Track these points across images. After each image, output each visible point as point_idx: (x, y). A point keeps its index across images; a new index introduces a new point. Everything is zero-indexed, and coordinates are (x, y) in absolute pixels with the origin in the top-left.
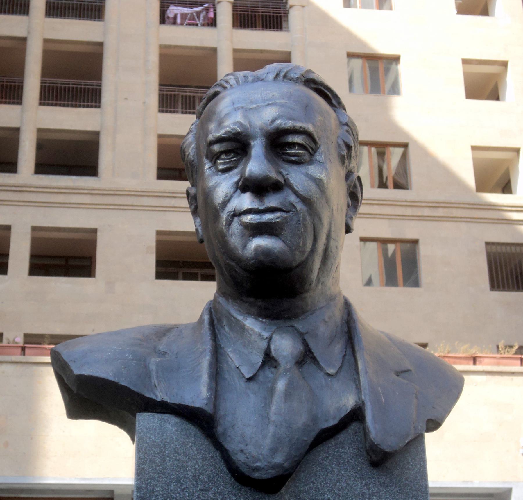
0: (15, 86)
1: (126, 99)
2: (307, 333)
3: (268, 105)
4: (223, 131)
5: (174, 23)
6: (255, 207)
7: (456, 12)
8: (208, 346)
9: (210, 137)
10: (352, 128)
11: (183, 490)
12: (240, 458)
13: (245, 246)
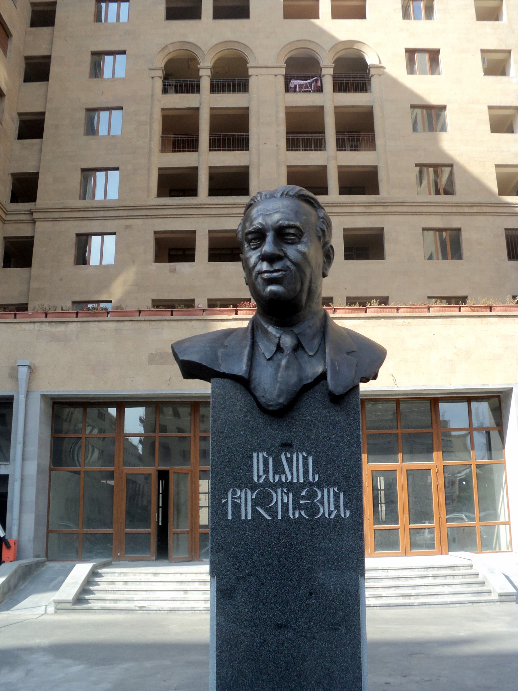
0: (193, 140)
1: (265, 143)
2: (299, 334)
3: (276, 212)
4: (252, 228)
5: (295, 91)
6: (268, 269)
7: (483, 74)
8: (249, 342)
9: (246, 231)
10: (326, 219)
11: (235, 416)
12: (262, 400)
13: (264, 290)
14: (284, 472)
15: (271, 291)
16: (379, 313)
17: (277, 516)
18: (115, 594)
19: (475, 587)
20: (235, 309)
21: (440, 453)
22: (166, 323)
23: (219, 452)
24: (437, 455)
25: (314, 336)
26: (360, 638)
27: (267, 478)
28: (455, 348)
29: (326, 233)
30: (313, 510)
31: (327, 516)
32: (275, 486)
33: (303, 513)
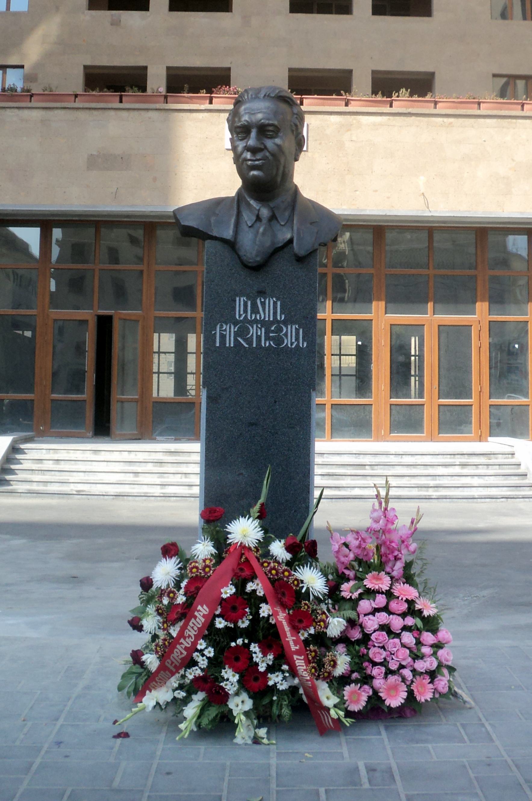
3: (259, 112)
4: (240, 124)
12: (245, 258)
13: (248, 174)
14: (259, 313)
15: (253, 175)
16: (409, 108)
17: (252, 345)
18: (44, 475)
19: (513, 480)
20: (209, 95)
21: (486, 305)
22: (112, 113)
23: (211, 296)
24: (482, 307)
25: (285, 209)
26: (310, 435)
27: (246, 317)
28: (513, 160)
29: (299, 127)
30: (279, 341)
31: (289, 346)
32: (252, 323)
33: (272, 343)
